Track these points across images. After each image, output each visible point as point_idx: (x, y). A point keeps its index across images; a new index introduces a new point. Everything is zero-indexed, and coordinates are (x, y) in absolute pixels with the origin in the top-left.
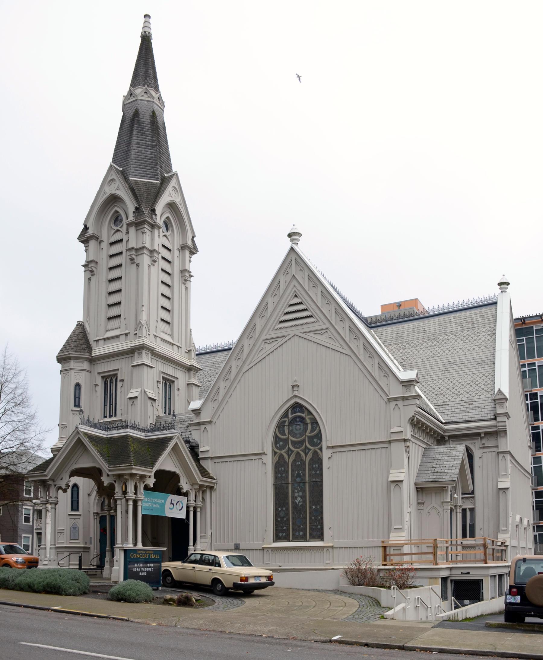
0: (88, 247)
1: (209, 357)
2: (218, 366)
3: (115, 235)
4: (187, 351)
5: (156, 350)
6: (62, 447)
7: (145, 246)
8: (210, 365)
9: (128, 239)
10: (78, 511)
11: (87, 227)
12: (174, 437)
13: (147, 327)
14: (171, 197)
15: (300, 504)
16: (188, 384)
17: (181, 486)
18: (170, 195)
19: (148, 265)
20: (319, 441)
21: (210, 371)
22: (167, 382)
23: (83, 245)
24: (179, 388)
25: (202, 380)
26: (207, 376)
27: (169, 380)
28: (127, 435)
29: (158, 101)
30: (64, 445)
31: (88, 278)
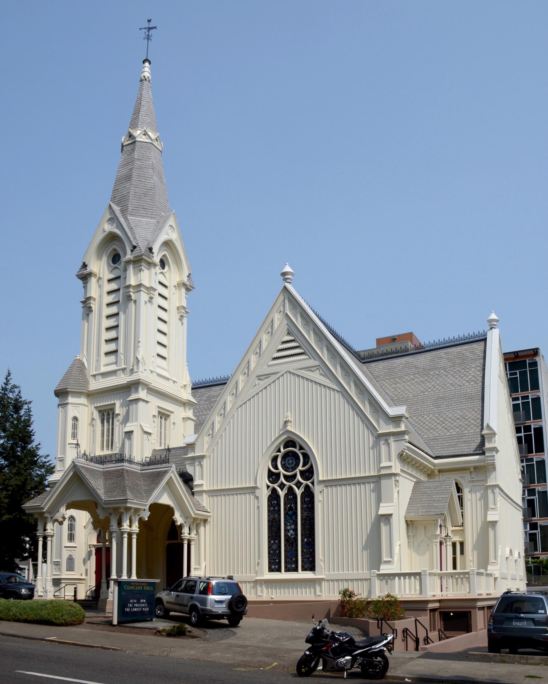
1: (205, 391)
4: (183, 386)
5: (152, 384)
8: (206, 399)
9: (126, 277)
11: (86, 264)
14: (168, 236)
15: (292, 537)
16: (183, 418)
18: (167, 233)
19: (145, 301)
20: (310, 475)
21: (206, 405)
23: (82, 281)
27: (164, 414)
28: (123, 469)
29: (156, 142)
31: (87, 314)
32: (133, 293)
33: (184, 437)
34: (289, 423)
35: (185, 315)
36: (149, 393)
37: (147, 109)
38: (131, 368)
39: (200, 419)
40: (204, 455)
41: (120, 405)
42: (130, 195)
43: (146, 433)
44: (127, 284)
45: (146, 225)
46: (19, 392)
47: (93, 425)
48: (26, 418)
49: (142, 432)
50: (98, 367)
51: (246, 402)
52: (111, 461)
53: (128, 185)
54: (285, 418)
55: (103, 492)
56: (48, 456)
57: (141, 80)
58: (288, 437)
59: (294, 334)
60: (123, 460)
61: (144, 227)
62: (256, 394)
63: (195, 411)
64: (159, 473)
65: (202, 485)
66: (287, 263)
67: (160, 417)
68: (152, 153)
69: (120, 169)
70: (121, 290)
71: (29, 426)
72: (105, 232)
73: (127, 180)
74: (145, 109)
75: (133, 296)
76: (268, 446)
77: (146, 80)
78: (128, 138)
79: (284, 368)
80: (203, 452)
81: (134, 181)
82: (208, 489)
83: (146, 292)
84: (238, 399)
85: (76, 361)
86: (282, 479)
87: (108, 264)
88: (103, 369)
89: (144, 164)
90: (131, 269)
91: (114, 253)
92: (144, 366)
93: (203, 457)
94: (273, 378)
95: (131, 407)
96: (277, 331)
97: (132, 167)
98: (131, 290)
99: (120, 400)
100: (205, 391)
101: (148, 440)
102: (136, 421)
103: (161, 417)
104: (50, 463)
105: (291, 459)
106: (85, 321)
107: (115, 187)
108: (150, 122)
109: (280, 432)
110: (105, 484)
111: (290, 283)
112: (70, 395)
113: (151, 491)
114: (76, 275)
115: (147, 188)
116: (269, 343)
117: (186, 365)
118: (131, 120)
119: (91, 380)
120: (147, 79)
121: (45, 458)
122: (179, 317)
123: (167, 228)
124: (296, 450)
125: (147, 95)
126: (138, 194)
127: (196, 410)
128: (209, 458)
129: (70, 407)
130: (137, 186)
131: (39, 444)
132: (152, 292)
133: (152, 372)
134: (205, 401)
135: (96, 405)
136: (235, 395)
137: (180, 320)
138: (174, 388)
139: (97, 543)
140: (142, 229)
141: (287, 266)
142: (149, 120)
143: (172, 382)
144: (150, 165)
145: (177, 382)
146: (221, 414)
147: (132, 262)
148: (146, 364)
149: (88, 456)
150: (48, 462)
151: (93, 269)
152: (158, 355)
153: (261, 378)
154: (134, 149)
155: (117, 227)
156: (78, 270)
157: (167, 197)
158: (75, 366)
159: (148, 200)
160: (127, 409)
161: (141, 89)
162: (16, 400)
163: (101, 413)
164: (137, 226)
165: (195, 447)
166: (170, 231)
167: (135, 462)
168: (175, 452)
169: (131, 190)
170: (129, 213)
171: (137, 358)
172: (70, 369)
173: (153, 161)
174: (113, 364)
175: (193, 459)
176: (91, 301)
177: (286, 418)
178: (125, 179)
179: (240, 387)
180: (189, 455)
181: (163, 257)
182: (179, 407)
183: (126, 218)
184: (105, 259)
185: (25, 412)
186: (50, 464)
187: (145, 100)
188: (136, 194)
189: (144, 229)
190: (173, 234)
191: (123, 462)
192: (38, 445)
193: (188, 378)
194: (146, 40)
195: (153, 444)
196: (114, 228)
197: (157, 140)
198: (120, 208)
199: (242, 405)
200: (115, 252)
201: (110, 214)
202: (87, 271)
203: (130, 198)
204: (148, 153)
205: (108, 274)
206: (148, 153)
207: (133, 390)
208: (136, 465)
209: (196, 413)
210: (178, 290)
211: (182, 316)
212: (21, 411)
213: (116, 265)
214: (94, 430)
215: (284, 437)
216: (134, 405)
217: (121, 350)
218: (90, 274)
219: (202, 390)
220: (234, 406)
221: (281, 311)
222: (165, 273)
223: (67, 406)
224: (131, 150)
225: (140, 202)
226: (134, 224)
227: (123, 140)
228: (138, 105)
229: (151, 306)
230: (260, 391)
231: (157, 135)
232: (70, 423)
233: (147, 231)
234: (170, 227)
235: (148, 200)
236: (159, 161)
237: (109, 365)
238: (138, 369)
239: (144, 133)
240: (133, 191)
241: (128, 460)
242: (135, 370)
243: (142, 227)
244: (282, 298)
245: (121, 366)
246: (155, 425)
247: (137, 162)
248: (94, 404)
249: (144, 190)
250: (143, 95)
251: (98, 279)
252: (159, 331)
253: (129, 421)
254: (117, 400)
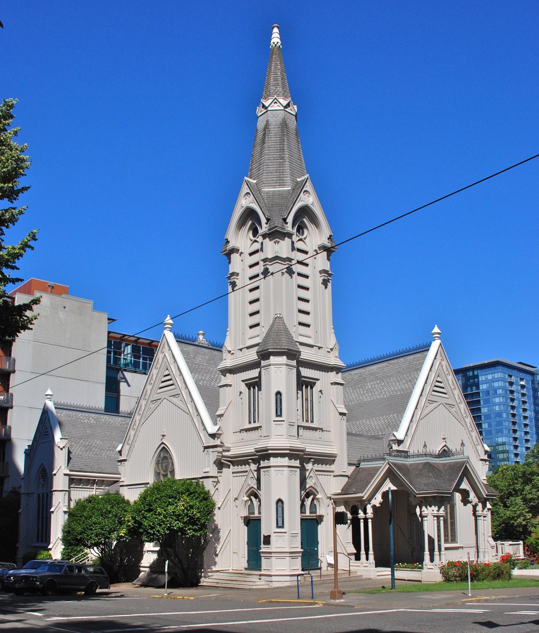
10: (284, 528)
17: (470, 500)
23: (227, 257)
139: (310, 514)
147: (267, 236)
222: (305, 239)
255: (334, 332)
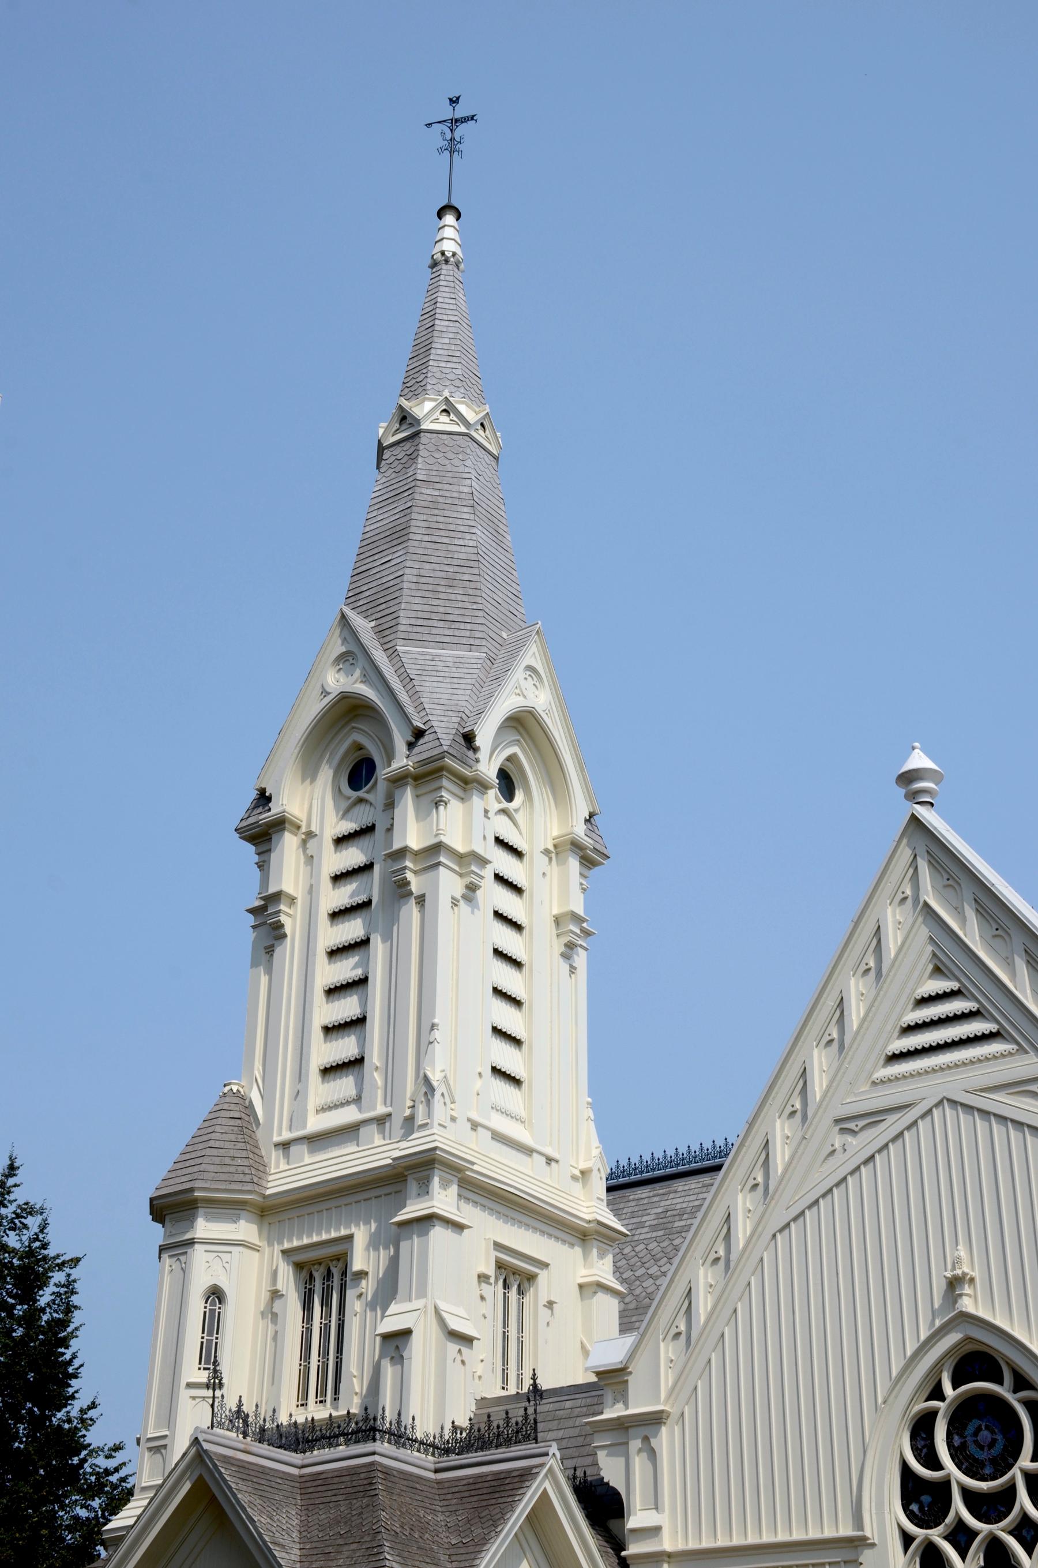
0: (266, 855)
1: (651, 1194)
2: (682, 1223)
3: (351, 812)
4: (578, 1173)
5: (475, 1167)
6: (132, 1526)
7: (441, 842)
8: (655, 1222)
9: (392, 825)
11: (267, 794)
12: (535, 1471)
13: (446, 1094)
14: (521, 698)
16: (581, 1286)
18: (518, 691)
19: (453, 898)
21: (655, 1244)
22: (511, 1278)
23: (253, 848)
24: (552, 1299)
25: (629, 1273)
26: (644, 1260)
27: (516, 1272)
28: (372, 1464)
29: (481, 432)
30: (147, 1507)
31: (266, 948)
32: (415, 872)
33: (586, 1352)
34: (966, 1286)
35: (580, 942)
36: (465, 1198)
37: (454, 341)
38: (408, 1112)
39: (637, 1292)
40: (662, 1411)
41: (368, 1239)
42: (405, 585)
43: (456, 1336)
44: (396, 846)
45: (454, 670)
46: (43, 1228)
47: (275, 1316)
48: (55, 1315)
49: (442, 1336)
50: (297, 1117)
51: (803, 1213)
52: (329, 1438)
53: (396, 555)
54: (949, 1267)
55: (297, 1559)
56: (117, 1448)
57: (434, 264)
58: (968, 1339)
59: (957, 973)
60: (374, 1429)
61: (447, 674)
62: (838, 1185)
63: (619, 1264)
64: (500, 1478)
65: (656, 1530)
66: (917, 744)
67: (501, 1282)
68: (468, 463)
69: (375, 514)
70: (377, 868)
71: (65, 1343)
72: (329, 693)
73: (395, 542)
74: (447, 341)
75: (416, 884)
76: (894, 1374)
77: (447, 261)
78: (398, 425)
79: (929, 1091)
80: (658, 1403)
81: (416, 544)
82: (680, 1546)
83: (456, 868)
84: (773, 1202)
85: (227, 1099)
86: (959, 1506)
87: (338, 792)
88: (315, 1123)
89: (447, 494)
90: (408, 801)
91: (357, 756)
92: (450, 1105)
93: (655, 1420)
94: (894, 1124)
95: (404, 1245)
96: (897, 963)
97: (409, 504)
98: (408, 863)
99: (367, 1222)
100: (651, 1194)
101: (463, 1362)
102: (422, 1294)
103: (505, 1281)
104: (122, 1473)
105: (987, 1428)
106: (262, 969)
107: (358, 565)
108: (460, 377)
109: (933, 1320)
110: (305, 1528)
111: (929, 807)
112: (201, 1211)
113: (471, 1549)
114: (236, 830)
115: (455, 562)
116: (872, 1006)
117: (588, 1103)
118: (404, 375)
119: (276, 1162)
120: (452, 259)
121: (108, 1457)
122: (563, 949)
123: (519, 674)
124: (1003, 1391)
125: (453, 301)
126: (431, 580)
127: (624, 1262)
128: (677, 1423)
129: (199, 1254)
130: (424, 558)
131: (93, 1406)
132: (473, 868)
133: (475, 1126)
134: (654, 1228)
135: (286, 1245)
136: (761, 1189)
137: (566, 956)
138: (548, 1181)
140: (440, 679)
141: (917, 751)
142: (459, 372)
143: (544, 1160)
144: (463, 496)
145: (557, 1161)
146: (717, 1260)
148: (457, 1099)
149: (250, 1419)
150: (117, 1470)
151: (288, 809)
152: (495, 1070)
153: (851, 1125)
154: (415, 454)
155: (365, 679)
156: (242, 814)
157: (518, 588)
158: (223, 1114)
159: (459, 597)
160: (392, 1253)
161: (433, 289)
162: (30, 1253)
163: (305, 1274)
164: (424, 673)
165: (627, 1381)
166: (528, 685)
167: (416, 1441)
168: (557, 1406)
169: (407, 571)
170: (400, 635)
171: (427, 1080)
172: (207, 1124)
173: (474, 484)
174: (348, 1103)
175: (623, 1426)
176: (282, 907)
177: (954, 1268)
178: (388, 539)
179: (779, 1161)
180: (608, 1414)
181: (508, 763)
182: (566, 1248)
183: (391, 651)
184: (326, 774)
185: (54, 1293)
186: (123, 1480)
187: (445, 317)
188: (423, 580)
189: (448, 680)
190: (537, 693)
191: (374, 1440)
192: (90, 1408)
193: (596, 1149)
194: (447, 153)
195: (480, 1377)
196: (355, 683)
197: (482, 425)
198: (373, 624)
199: (788, 1225)
200: (356, 754)
201: (344, 641)
202: (269, 814)
203: (405, 592)
204: (456, 462)
205: (335, 820)
206: (456, 462)
207: (412, 1186)
208: (419, 1451)
209: (621, 1270)
210: (558, 864)
211: (570, 946)
212: (41, 1292)
213: (361, 794)
214: (276, 1332)
215: (953, 1338)
216: (416, 1239)
217: (374, 1058)
218: (280, 824)
219: (642, 1193)
220: (760, 1229)
221: (905, 899)
222: (516, 810)
223: (189, 1251)
224: (407, 458)
225: (436, 602)
226: (418, 667)
227: (381, 431)
228: (425, 332)
229: (473, 912)
230: (852, 1173)
231: (486, 412)
232: (196, 1308)
233: (457, 686)
234: (528, 673)
235: (459, 597)
236: (490, 486)
237: (336, 1106)
238: (429, 1115)
239: (444, 407)
240: (415, 572)
241: (391, 1433)
242: (420, 1120)
243: (442, 674)
244: (905, 854)
245: (375, 1108)
246: (486, 1308)
247: (424, 491)
248: (281, 1242)
249: (446, 568)
250: (438, 305)
251: (303, 837)
252: (497, 992)
253: (398, 1297)
254: (357, 1225)
255: (593, 1118)
